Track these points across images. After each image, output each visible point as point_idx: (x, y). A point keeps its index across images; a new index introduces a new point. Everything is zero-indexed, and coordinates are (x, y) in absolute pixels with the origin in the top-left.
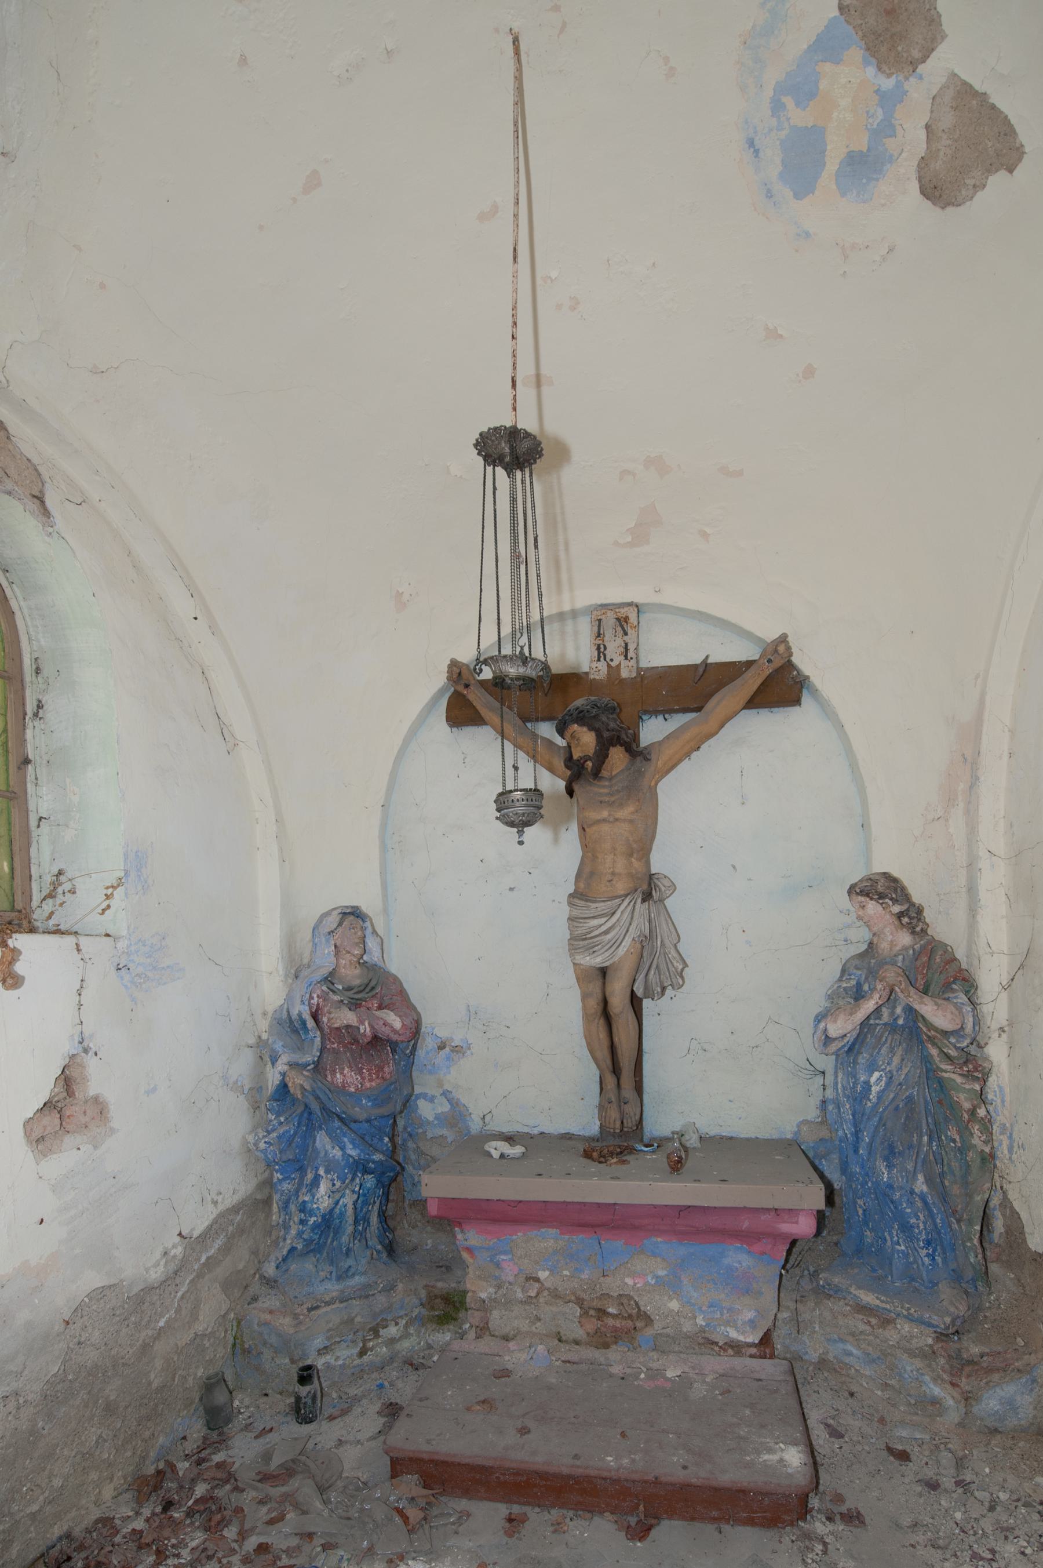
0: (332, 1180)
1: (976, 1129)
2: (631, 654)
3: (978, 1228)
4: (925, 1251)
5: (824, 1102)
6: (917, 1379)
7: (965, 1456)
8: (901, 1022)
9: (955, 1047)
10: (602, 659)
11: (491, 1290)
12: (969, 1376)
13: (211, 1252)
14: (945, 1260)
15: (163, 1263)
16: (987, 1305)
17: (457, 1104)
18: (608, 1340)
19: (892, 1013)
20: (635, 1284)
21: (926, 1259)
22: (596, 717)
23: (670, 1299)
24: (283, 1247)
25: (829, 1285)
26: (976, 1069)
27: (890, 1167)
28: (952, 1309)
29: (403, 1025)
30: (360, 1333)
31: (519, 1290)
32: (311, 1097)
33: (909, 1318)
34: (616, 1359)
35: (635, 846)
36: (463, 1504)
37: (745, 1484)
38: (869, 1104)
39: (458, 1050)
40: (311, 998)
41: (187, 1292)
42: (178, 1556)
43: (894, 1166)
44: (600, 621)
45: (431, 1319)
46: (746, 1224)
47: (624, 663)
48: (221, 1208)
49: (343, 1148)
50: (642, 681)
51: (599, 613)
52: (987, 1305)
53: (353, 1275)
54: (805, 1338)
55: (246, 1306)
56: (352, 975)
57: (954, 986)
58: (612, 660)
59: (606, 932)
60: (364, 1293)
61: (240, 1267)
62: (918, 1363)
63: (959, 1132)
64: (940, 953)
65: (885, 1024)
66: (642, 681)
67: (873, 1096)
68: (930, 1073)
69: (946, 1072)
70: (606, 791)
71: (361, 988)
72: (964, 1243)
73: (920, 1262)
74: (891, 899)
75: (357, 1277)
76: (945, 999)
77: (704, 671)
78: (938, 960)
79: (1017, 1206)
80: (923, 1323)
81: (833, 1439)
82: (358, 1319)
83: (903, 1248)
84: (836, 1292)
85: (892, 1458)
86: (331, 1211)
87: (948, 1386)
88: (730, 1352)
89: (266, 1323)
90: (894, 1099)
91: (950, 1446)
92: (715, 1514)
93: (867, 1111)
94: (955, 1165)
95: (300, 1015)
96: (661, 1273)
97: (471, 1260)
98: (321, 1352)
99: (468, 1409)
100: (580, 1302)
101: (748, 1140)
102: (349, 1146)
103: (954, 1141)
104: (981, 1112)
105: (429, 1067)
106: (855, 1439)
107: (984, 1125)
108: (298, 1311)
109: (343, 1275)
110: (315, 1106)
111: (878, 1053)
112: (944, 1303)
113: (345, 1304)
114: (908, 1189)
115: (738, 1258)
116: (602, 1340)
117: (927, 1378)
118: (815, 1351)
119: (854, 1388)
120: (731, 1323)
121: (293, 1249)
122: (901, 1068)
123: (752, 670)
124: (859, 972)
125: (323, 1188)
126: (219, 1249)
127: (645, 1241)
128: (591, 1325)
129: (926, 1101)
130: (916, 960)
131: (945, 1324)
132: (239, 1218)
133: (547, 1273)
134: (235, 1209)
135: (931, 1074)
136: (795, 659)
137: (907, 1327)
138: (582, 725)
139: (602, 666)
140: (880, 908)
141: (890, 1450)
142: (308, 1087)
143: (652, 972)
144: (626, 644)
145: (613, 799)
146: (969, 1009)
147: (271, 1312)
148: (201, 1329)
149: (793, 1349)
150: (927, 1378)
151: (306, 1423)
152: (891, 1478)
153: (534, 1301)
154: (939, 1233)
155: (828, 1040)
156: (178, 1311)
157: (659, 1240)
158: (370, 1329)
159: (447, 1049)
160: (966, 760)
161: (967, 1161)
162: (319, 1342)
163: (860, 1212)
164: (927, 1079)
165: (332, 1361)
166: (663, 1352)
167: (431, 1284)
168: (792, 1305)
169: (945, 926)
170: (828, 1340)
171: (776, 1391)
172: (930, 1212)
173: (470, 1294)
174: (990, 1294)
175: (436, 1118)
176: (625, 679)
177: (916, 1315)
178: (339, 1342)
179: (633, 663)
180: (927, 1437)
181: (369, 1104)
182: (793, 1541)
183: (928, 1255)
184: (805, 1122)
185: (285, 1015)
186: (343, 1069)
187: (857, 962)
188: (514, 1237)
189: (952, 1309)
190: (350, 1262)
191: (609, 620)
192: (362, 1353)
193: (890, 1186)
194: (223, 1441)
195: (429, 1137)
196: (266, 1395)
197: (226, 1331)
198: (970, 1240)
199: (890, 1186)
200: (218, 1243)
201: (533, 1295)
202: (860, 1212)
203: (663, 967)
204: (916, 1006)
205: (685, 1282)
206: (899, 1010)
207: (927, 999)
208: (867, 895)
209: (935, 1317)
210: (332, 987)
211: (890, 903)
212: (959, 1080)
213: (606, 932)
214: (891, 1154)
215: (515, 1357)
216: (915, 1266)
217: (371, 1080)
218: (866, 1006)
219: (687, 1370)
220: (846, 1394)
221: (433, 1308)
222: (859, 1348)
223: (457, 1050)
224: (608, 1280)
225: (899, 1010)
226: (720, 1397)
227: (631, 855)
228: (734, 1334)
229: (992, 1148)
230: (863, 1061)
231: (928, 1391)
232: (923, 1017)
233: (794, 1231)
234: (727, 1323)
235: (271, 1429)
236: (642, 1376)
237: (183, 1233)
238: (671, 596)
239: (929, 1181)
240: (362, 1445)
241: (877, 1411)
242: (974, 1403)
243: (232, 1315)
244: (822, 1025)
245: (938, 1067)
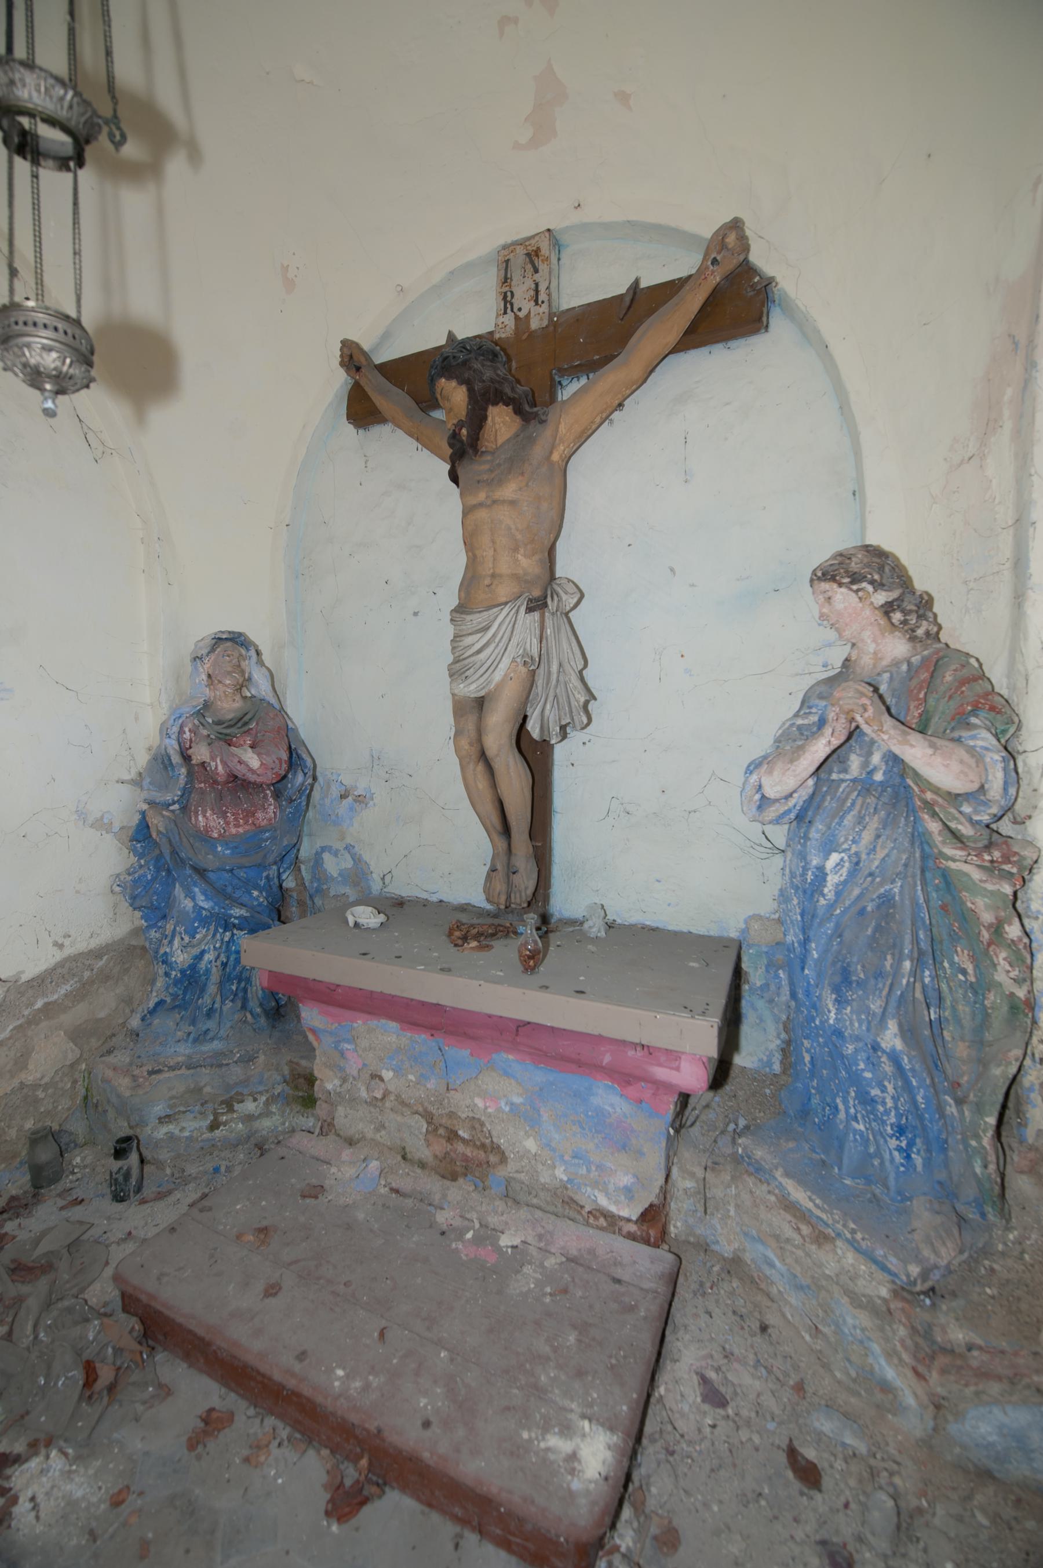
1: (1001, 956)
2: (542, 297)
3: (992, 1120)
4: (893, 1143)
6: (861, 1342)
7: (920, 1511)
8: (879, 777)
9: (970, 820)
10: (509, 310)
11: (337, 1082)
12: (943, 1372)
14: (928, 1163)
16: (1000, 1247)
17: (360, 860)
18: (458, 1169)
19: (866, 763)
20: (486, 1108)
21: (896, 1154)
22: (465, 363)
23: (527, 1135)
25: (749, 1157)
26: (1006, 859)
28: (926, 1252)
29: (262, 764)
30: (210, 1105)
31: (363, 1088)
32: (164, 840)
33: (852, 1243)
34: (454, 1204)
35: (519, 537)
37: (494, 1490)
39: (361, 800)
40: (181, 732)
43: (848, 1002)
44: (507, 261)
47: (535, 310)
48: (68, 951)
49: (193, 899)
50: (555, 330)
51: (506, 252)
52: (1000, 1247)
53: (212, 1039)
54: (715, 1222)
56: (230, 706)
57: (974, 720)
58: (520, 309)
59: (479, 652)
60: (217, 1062)
61: (102, 1015)
62: (864, 1319)
63: (973, 958)
64: (954, 667)
65: (854, 781)
66: (555, 330)
67: (829, 889)
68: (928, 861)
69: (954, 860)
70: (486, 467)
71: (231, 723)
72: (965, 1141)
73: (887, 1156)
74: (872, 582)
75: (216, 1042)
76: (952, 740)
77: (632, 300)
78: (948, 678)
80: (875, 1261)
81: (706, 1407)
82: (208, 1089)
83: (861, 1127)
85: (790, 1474)
86: (193, 967)
87: (910, 1374)
88: (602, 1222)
90: (859, 897)
91: (897, 1480)
92: (458, 1511)
93: (820, 912)
94: (964, 1009)
96: (517, 1100)
98: (164, 1120)
100: (429, 1117)
101: (676, 934)
103: (964, 972)
104: (1013, 931)
105: (333, 817)
106: (745, 1413)
107: (1017, 952)
108: (136, 1072)
109: (201, 1038)
111: (839, 824)
112: (916, 1236)
113: (192, 1071)
114: (869, 1041)
115: (609, 1099)
116: (451, 1170)
117: (876, 1348)
118: (730, 1242)
119: (771, 1319)
121: (160, 1003)
122: (874, 849)
126: (66, 995)
127: (494, 1056)
128: (440, 1147)
129: (914, 901)
130: (911, 680)
131: (908, 1276)
132: (101, 963)
135: (931, 863)
136: (756, 257)
138: (449, 378)
139: (509, 320)
140: (853, 598)
141: (792, 1453)
143: (548, 707)
144: (537, 285)
145: (493, 475)
146: (997, 757)
148: (31, 1078)
149: (698, 1232)
150: (876, 1348)
152: (776, 1518)
153: (379, 1104)
154: (921, 1118)
155: (764, 802)
157: (510, 1057)
158: (222, 1103)
159: (350, 798)
160: (1016, 344)
162: (159, 1109)
163: (807, 1058)
164: (923, 871)
165: (177, 1132)
166: (517, 1202)
168: (700, 1173)
169: (964, 627)
170: (746, 1234)
171: (632, 1309)
172: (907, 1082)
173: (317, 1082)
174: (1008, 1229)
175: (340, 874)
176: (535, 331)
177: (864, 1244)
178: (184, 1112)
179: (544, 308)
180: (862, 1448)
183: (899, 1149)
185: (163, 752)
186: (206, 811)
187: (823, 688)
188: (355, 1025)
189: (926, 1252)
190: (211, 1024)
191: (519, 257)
192: (214, 1126)
195: (331, 895)
197: (75, 1082)
198: (977, 1137)
199: (839, 1033)
201: (379, 1096)
202: (807, 1058)
203: (563, 699)
204: (897, 750)
205: (545, 1117)
206: (876, 759)
207: (915, 737)
208: (833, 579)
209: (894, 1260)
210: (202, 720)
211: (870, 588)
212: (976, 875)
213: (479, 652)
214: (844, 982)
216: (876, 1162)
217: (237, 826)
218: (813, 749)
219: (530, 1240)
220: (756, 1326)
222: (783, 1260)
223: (360, 800)
225: (876, 759)
226: (548, 1300)
227: (516, 550)
228: (603, 1202)
229: (1030, 992)
230: (817, 836)
231: (877, 1367)
232: (914, 770)
234: (595, 1185)
235: (83, 1200)
236: (469, 1235)
239: (908, 1032)
241: (796, 1368)
242: (950, 1418)
243: (84, 1066)
244: (754, 778)
245: (941, 853)
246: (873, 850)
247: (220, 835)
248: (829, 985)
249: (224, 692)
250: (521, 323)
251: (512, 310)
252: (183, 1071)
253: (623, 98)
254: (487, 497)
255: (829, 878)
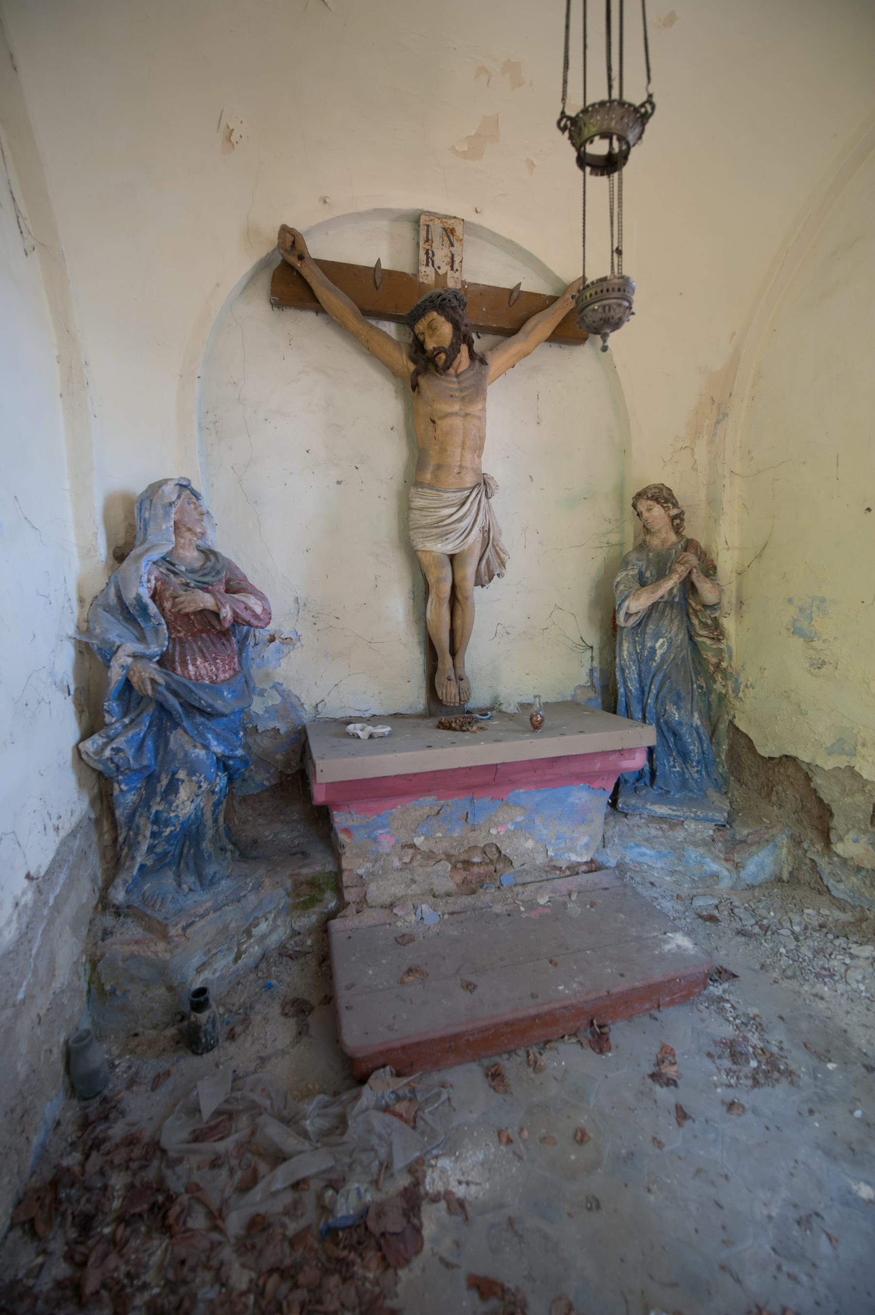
0: (199, 782)
2: (456, 266)
5: (591, 670)
13: (57, 891)
15: (15, 917)
21: (696, 775)
23: (527, 839)
24: (131, 867)
27: (679, 709)
30: (235, 939)
33: (697, 819)
36: (436, 1077)
38: (654, 664)
41: (40, 947)
42: (145, 1286)
45: (295, 907)
46: (598, 766)
47: (450, 274)
48: (63, 834)
49: (206, 747)
55: (100, 943)
59: (460, 520)
62: (701, 850)
63: (705, 681)
79: (742, 727)
82: (233, 925)
83: (678, 769)
84: (634, 810)
85: (708, 923)
87: (723, 862)
89: (133, 956)
95: (139, 598)
96: (519, 819)
97: (348, 841)
98: (199, 970)
99: (402, 982)
100: (449, 857)
102: (214, 743)
110: (173, 702)
112: (716, 803)
113: (218, 913)
116: (470, 888)
120: (571, 850)
121: (142, 867)
123: (557, 305)
124: (640, 563)
125: (184, 793)
127: (510, 794)
132: (77, 843)
133: (422, 838)
134: (73, 834)
137: (693, 826)
140: (662, 511)
141: (700, 916)
142: (161, 681)
144: (453, 255)
147: (137, 942)
151: (208, 1051)
156: (35, 973)
157: (522, 791)
158: (244, 932)
161: (709, 702)
162: (196, 961)
167: (296, 872)
177: (702, 815)
179: (457, 274)
181: (230, 696)
182: (707, 1008)
183: (697, 772)
184: (580, 687)
188: (394, 810)
193: (680, 723)
194: (109, 1110)
196: (136, 1035)
198: (719, 756)
200: (62, 878)
213: (460, 520)
215: (406, 920)
217: (224, 672)
221: (298, 895)
224: (476, 833)
226: (593, 910)
230: (650, 631)
231: (708, 869)
233: (631, 766)
237: (33, 873)
238: (489, 220)
240: (288, 1053)
246: (677, 635)
247: (212, 682)
248: (670, 702)
249: (190, 540)
250: (440, 278)
251: (433, 265)
252: (212, 915)
253: (531, 165)
254: (461, 409)
255: (658, 652)
